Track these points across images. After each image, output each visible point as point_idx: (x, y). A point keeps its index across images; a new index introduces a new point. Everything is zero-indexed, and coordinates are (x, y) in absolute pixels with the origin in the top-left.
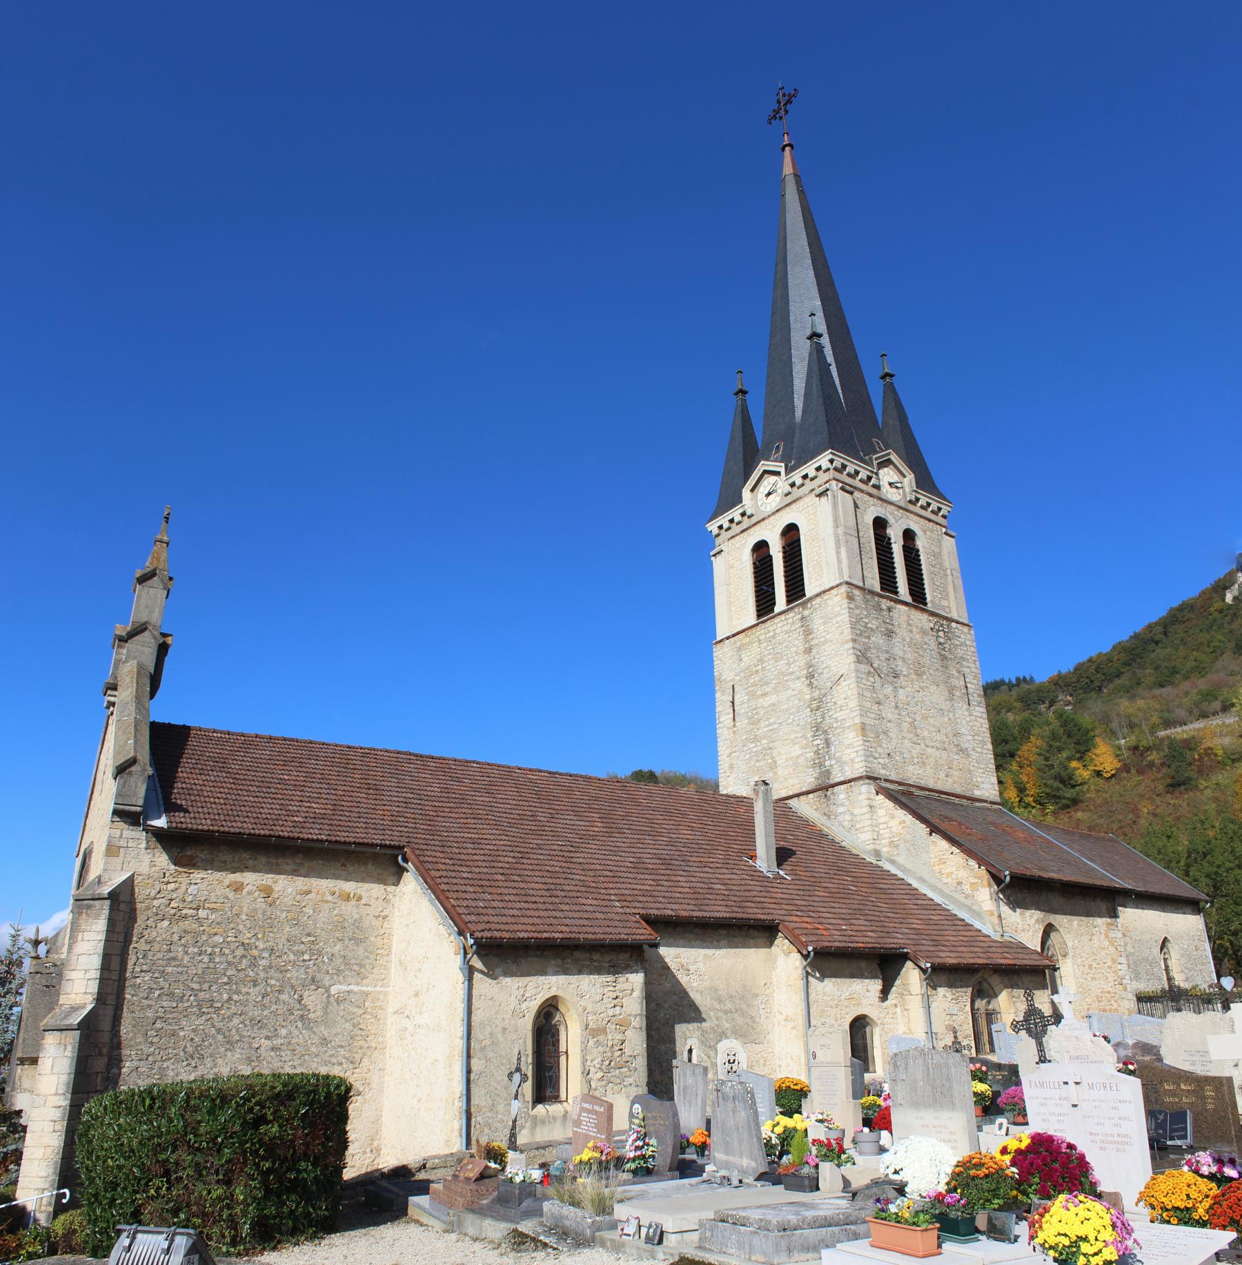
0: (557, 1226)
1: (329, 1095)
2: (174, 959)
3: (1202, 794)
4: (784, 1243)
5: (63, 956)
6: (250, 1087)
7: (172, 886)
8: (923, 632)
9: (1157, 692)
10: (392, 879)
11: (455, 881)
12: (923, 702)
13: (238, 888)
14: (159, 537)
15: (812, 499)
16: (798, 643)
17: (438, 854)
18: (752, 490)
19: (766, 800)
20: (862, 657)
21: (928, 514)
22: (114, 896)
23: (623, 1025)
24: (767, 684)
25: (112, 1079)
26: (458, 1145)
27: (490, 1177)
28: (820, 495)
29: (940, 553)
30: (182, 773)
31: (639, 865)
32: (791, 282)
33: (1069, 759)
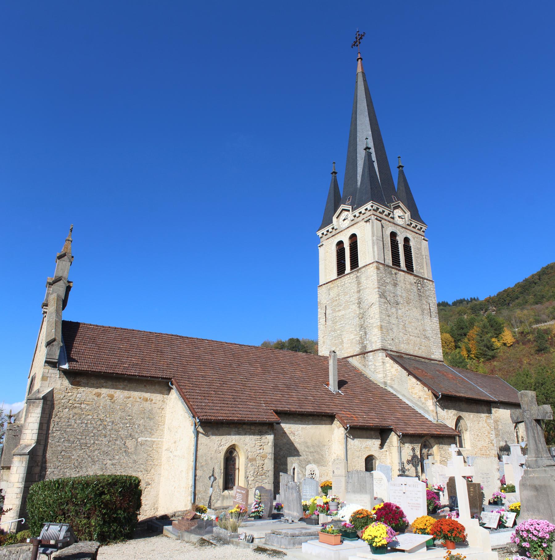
0: (218, 537)
1: (131, 484)
2: (70, 425)
3: (552, 355)
4: (292, 541)
5: (22, 422)
6: (98, 480)
7: (70, 394)
8: (411, 284)
9: (533, 307)
10: (166, 392)
11: (193, 394)
12: (409, 316)
13: (99, 395)
14: (67, 238)
15: (363, 223)
16: (355, 288)
17: (186, 382)
18: (337, 218)
19: (334, 360)
20: (382, 295)
21: (416, 230)
22: (45, 398)
23: (264, 457)
24: (341, 306)
25: (42, 476)
26: (189, 507)
27: (197, 518)
28: (366, 222)
29: (420, 248)
30: (75, 344)
31: (276, 388)
32: (358, 122)
33: (491, 337)
